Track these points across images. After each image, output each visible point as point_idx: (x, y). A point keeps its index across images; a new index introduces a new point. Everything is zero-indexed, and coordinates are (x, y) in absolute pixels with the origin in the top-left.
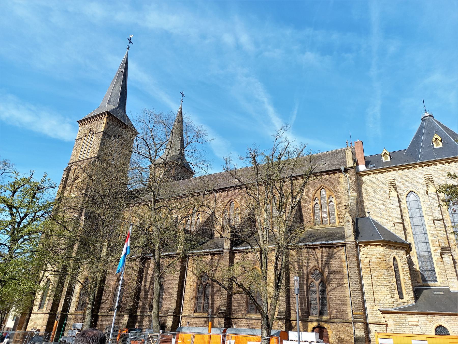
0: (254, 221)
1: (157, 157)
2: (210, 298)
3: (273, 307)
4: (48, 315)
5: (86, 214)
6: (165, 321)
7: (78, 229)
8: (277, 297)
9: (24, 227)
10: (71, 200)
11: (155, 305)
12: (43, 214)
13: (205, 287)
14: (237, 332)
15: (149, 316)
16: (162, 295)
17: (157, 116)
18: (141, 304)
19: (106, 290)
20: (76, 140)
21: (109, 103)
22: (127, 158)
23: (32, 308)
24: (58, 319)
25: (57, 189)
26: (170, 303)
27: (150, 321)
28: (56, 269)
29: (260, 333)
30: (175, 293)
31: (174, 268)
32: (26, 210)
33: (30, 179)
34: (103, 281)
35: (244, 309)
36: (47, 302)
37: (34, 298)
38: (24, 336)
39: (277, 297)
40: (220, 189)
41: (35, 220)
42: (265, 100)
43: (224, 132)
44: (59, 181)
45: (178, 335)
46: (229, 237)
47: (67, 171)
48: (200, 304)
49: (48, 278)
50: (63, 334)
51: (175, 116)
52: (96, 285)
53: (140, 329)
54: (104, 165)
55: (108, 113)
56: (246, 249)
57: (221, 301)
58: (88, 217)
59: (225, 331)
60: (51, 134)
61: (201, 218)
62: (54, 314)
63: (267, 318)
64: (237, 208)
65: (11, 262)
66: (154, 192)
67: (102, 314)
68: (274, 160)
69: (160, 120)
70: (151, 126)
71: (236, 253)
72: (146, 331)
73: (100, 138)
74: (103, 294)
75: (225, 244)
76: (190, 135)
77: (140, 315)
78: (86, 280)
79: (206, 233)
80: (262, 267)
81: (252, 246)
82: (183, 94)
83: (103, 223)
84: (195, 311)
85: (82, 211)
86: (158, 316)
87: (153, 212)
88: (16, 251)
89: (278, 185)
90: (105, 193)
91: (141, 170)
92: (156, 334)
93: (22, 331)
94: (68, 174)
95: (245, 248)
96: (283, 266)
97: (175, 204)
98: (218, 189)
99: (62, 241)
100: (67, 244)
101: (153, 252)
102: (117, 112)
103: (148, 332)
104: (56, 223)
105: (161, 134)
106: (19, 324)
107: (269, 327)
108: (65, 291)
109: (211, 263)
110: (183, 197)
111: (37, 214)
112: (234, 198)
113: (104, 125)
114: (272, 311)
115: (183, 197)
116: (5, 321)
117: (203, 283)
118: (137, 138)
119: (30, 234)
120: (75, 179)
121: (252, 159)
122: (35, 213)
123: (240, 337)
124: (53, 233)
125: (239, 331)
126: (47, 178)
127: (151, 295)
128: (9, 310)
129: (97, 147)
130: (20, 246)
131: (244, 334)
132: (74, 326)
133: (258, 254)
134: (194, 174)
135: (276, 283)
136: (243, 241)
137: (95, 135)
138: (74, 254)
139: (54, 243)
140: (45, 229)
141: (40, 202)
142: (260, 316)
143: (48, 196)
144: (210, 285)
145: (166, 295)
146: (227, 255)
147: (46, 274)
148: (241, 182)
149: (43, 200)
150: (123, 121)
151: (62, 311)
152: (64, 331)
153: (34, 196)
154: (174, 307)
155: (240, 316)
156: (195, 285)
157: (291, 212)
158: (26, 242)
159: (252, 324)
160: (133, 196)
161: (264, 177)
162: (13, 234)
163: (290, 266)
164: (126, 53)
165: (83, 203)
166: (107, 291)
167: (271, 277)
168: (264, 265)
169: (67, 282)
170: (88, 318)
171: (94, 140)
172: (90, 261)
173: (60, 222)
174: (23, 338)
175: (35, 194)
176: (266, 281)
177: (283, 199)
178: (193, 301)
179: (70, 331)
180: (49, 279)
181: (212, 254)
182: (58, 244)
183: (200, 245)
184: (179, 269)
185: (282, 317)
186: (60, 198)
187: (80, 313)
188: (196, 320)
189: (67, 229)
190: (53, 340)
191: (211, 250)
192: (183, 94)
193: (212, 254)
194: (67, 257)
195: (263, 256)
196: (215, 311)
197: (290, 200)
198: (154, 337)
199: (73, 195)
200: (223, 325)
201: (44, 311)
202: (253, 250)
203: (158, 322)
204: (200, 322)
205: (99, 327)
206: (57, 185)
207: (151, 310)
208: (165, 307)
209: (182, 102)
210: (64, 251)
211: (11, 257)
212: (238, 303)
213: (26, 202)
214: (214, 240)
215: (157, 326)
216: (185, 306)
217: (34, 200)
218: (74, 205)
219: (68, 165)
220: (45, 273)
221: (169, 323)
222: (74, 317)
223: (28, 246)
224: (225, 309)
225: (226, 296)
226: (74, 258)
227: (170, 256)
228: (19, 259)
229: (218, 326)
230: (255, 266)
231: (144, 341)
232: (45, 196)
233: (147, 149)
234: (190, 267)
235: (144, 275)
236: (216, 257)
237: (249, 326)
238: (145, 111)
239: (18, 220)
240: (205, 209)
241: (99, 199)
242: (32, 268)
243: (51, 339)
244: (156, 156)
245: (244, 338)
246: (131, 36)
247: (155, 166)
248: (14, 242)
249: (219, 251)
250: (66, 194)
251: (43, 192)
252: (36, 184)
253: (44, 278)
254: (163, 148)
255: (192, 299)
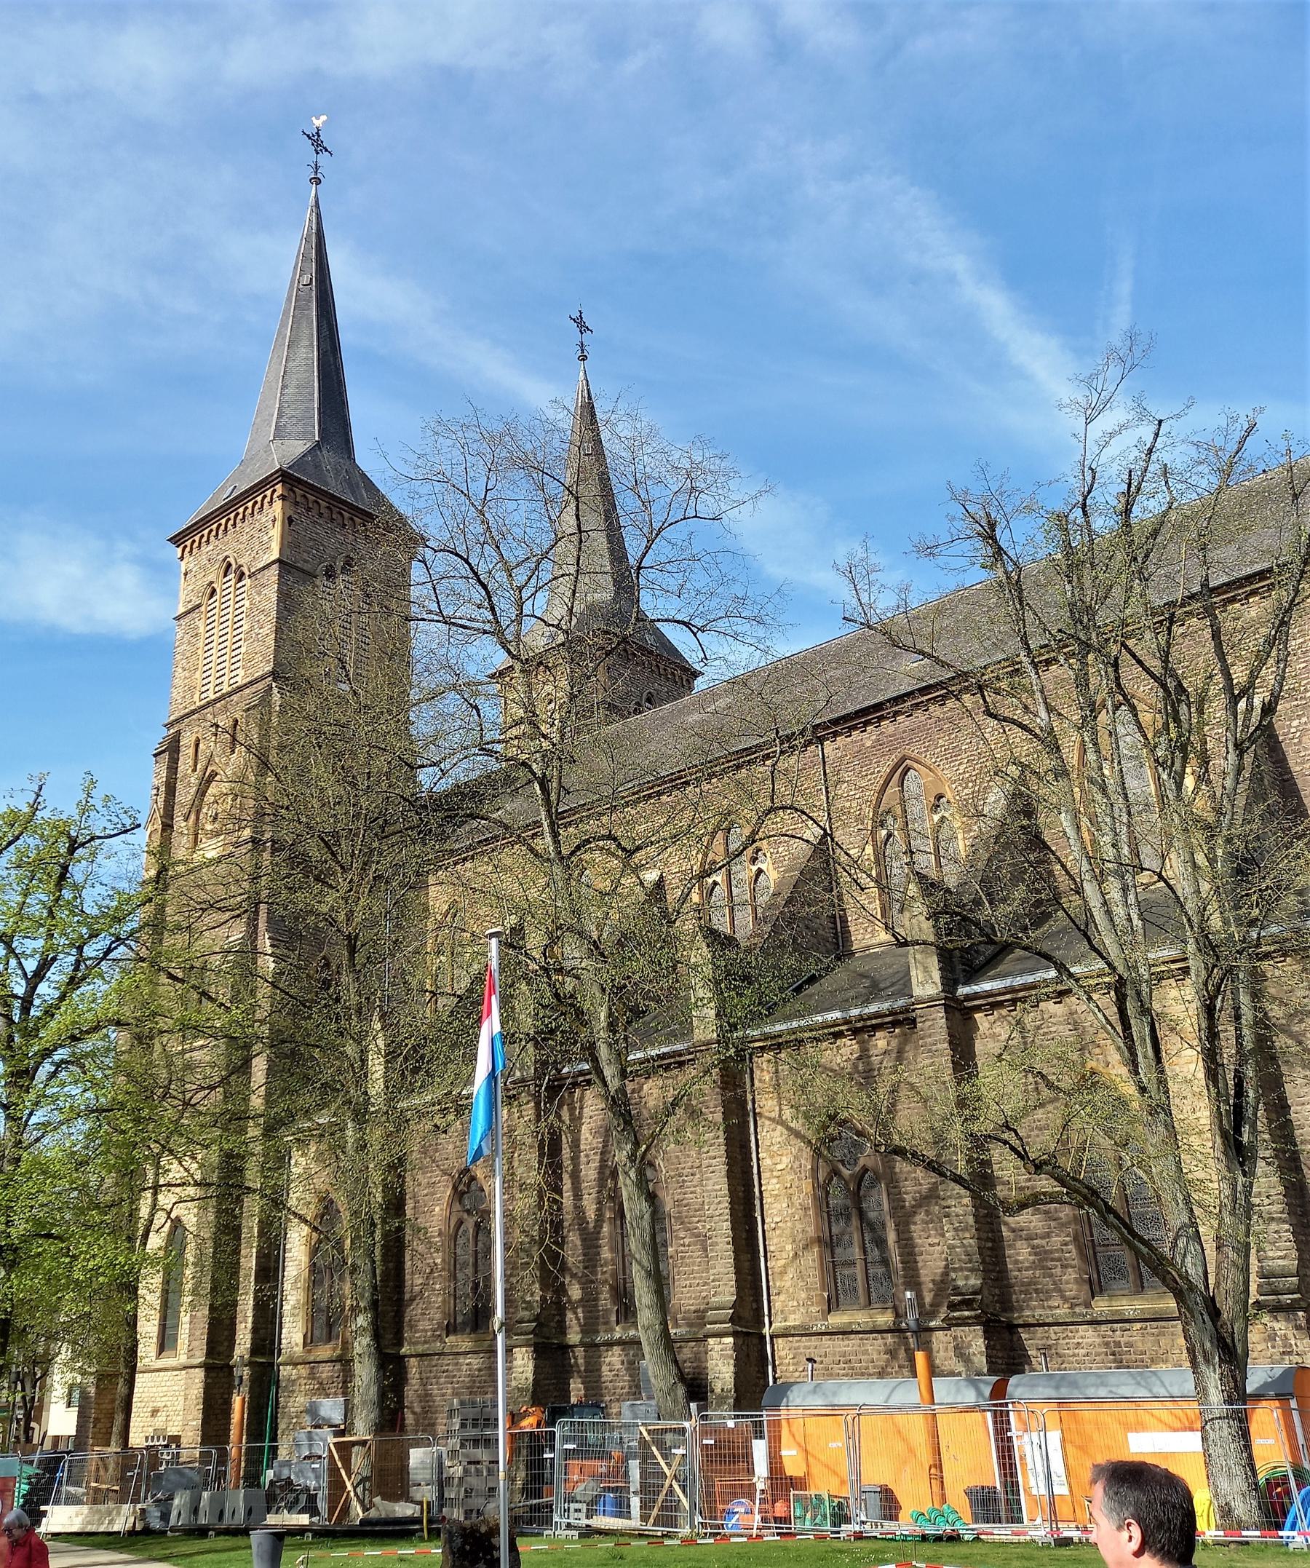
0: (1037, 842)
1: (528, 623)
2: (891, 1237)
3: (1232, 1255)
4: (199, 1374)
5: (275, 926)
6: (700, 1359)
7: (253, 992)
8: (1243, 1208)
9: (49, 1013)
10: (206, 874)
11: (643, 1293)
12: (109, 950)
13: (854, 1192)
14: (1064, 1392)
15: (620, 1342)
16: (665, 1245)
17: (494, 439)
18: (575, 1292)
19: (415, 1246)
20: (178, 618)
21: (279, 434)
22: (397, 653)
23: (133, 1351)
24: (243, 1387)
25: (141, 838)
26: (707, 1280)
27: (632, 1366)
28: (198, 1177)
29: (1189, 1387)
30: (721, 1230)
31: (694, 1113)
32: (40, 943)
33: (34, 808)
34: (395, 1205)
35: (1071, 1275)
36: (185, 1318)
37: (136, 1308)
38: (124, 1471)
39: (1243, 1208)
40: (846, 718)
41: (84, 978)
42: (960, 264)
43: (788, 461)
44: (145, 802)
45: (776, 1424)
46: (932, 939)
47: (166, 755)
48: (846, 1272)
49: (173, 1215)
50: (274, 1450)
51: (566, 421)
52: (373, 1225)
53: (594, 1404)
54: (311, 704)
55: (284, 476)
56: (1026, 987)
57: (951, 1247)
58: (286, 936)
59: (999, 1391)
60: (73, 622)
61: (774, 868)
62: (222, 1368)
63: (1215, 1313)
64: (940, 797)
65: (24, 1166)
66: (543, 782)
67: (420, 1349)
68: (1098, 523)
69: (510, 453)
70: (477, 488)
71: (978, 1009)
72: (623, 1412)
73: (271, 593)
74: (408, 1264)
75: (916, 974)
76: (655, 492)
77: (582, 1344)
78: (328, 1208)
79: (810, 932)
80: (1133, 1064)
81: (1061, 968)
82: (580, 323)
83: (352, 951)
84: (832, 1305)
85: (257, 912)
86: (668, 1342)
87: (557, 870)
88: (33, 1120)
89: (1146, 646)
90: (337, 823)
91: (467, 689)
92: (673, 1424)
93: (114, 1448)
94: (173, 768)
95: (1019, 981)
96: (1248, 1044)
97: (644, 821)
98: (835, 722)
99: (205, 1053)
100: (222, 1061)
101: (590, 1051)
102: (317, 466)
103: (633, 1421)
104: (163, 979)
105: (523, 515)
106: (97, 1420)
107: (1232, 1356)
108: (249, 1261)
109: (865, 1074)
110: (677, 782)
111: (89, 951)
112: (913, 750)
113: (276, 532)
114: (1233, 1275)
115: (677, 782)
116: (41, 1408)
117: (846, 1172)
118: (429, 554)
119: (74, 1038)
120: (207, 780)
121: (979, 544)
122: (80, 949)
123: (1087, 1412)
124: (163, 1023)
125: (1074, 1384)
126: (98, 794)
127: (613, 1250)
128: (46, 1361)
129: (265, 631)
130: (45, 1096)
131: (1102, 1401)
132: (312, 1411)
133: (1107, 1001)
134: (696, 674)
135: (1224, 1135)
136: (1006, 948)
137: (247, 581)
138: (257, 1102)
139: (169, 1065)
140: (127, 1013)
141: (92, 900)
142: (1171, 1304)
143: (118, 868)
144: (877, 1178)
145: (679, 1245)
146: (935, 1024)
147: (165, 1199)
148: (944, 665)
149: (99, 889)
150: (351, 500)
151: (254, 1351)
152: (274, 1439)
153: (62, 877)
154: (726, 1293)
155: (1062, 1312)
156: (807, 1186)
157: (1240, 769)
158: (63, 1075)
159: (1130, 1345)
160: (453, 816)
161: (1058, 619)
162: (9, 1047)
163: (1281, 1041)
164: (312, 200)
165: (255, 879)
166: (421, 1248)
167: (1196, 1110)
168: (1144, 1051)
169: (251, 1227)
170: (365, 1372)
171: (246, 603)
172: (331, 1124)
173: (180, 975)
174: (123, 1480)
175: (65, 868)
176: (1170, 1127)
177: (1183, 709)
178: (811, 1259)
179: (302, 1435)
180: (178, 1219)
181: (862, 1030)
182: (189, 1067)
183: (798, 990)
184: (718, 1117)
185: (1287, 1298)
186: (163, 870)
187: (324, 1352)
188: (841, 1345)
189: (210, 998)
190: (238, 1478)
191: (855, 1012)
192: (580, 323)
193: (862, 1030)
194: (235, 1119)
195: (1131, 1006)
196: (928, 1298)
197: (1216, 709)
198: (669, 1437)
199: (211, 849)
200: (981, 1361)
201: (183, 1359)
202: (1071, 984)
203: (673, 1368)
204: (865, 1352)
205: (418, 1410)
206: (142, 820)
207: (627, 1312)
208: (685, 1296)
209: (584, 358)
210: (218, 1094)
211: (18, 1144)
212: (1036, 1250)
213: (36, 908)
214: (855, 964)
215: (671, 1390)
216: (777, 1284)
217: (67, 894)
218: (221, 891)
219: (165, 732)
220: (160, 1197)
221: (721, 1367)
222: (303, 1371)
223: (75, 1090)
224: (975, 1281)
225: (971, 1220)
226: (262, 1120)
227: (674, 1062)
228: (51, 1147)
229: (960, 1368)
230: (1091, 1064)
231: (625, 1459)
232: (101, 871)
233: (478, 594)
234: (767, 1104)
235: (567, 1163)
236: (881, 1042)
237: (1118, 1358)
238: (439, 429)
239: (20, 989)
240: (785, 820)
241: (316, 852)
242: (103, 1180)
243: (231, 1476)
244: (520, 614)
245: (1104, 1417)
246: (317, 123)
247: (534, 665)
248: (21, 1082)
249: (892, 1013)
250: (180, 850)
251: (94, 854)
252: (61, 829)
253: (160, 1218)
254: (545, 576)
255: (806, 1247)
